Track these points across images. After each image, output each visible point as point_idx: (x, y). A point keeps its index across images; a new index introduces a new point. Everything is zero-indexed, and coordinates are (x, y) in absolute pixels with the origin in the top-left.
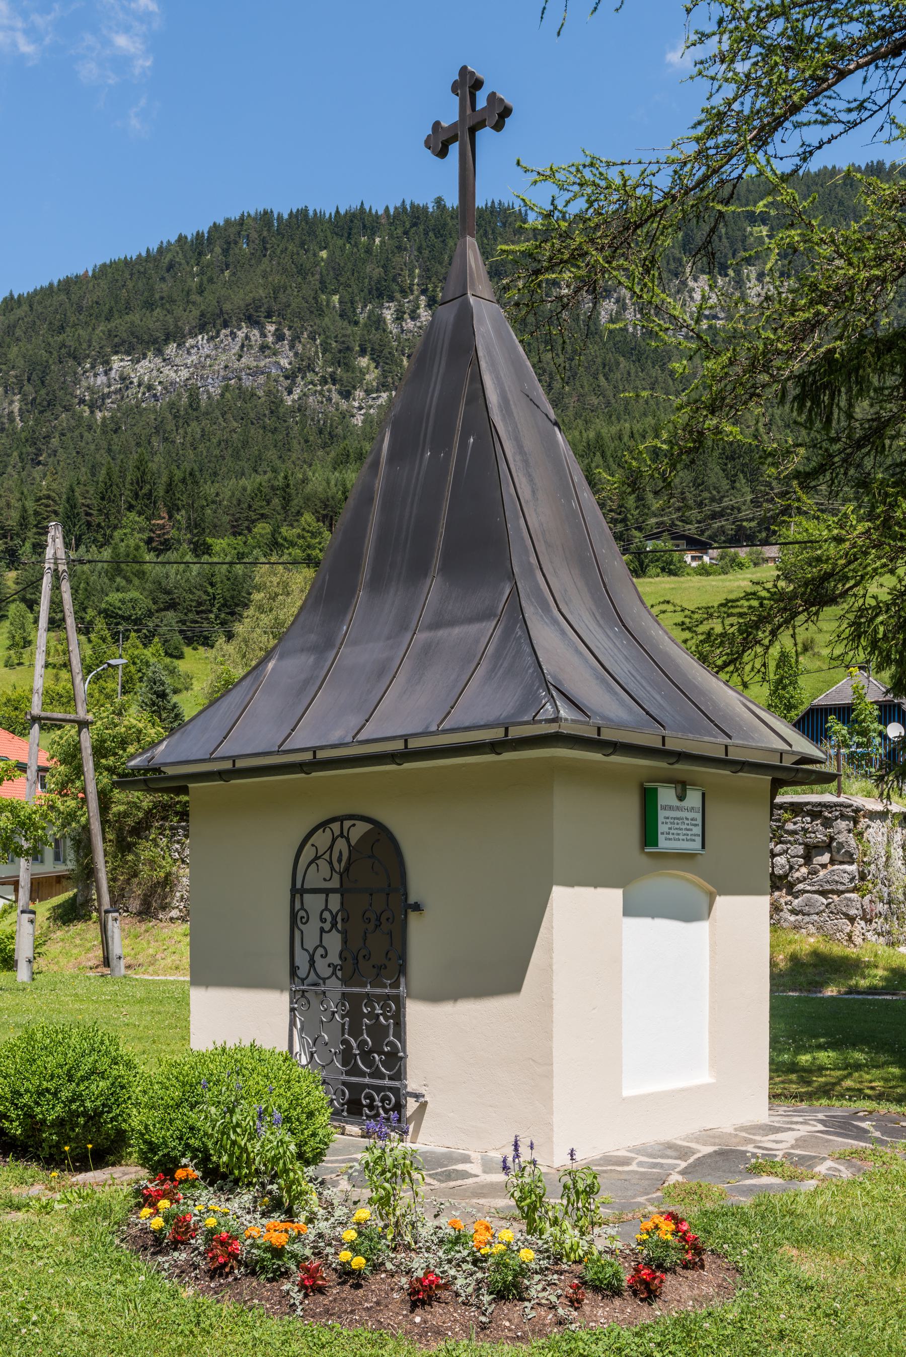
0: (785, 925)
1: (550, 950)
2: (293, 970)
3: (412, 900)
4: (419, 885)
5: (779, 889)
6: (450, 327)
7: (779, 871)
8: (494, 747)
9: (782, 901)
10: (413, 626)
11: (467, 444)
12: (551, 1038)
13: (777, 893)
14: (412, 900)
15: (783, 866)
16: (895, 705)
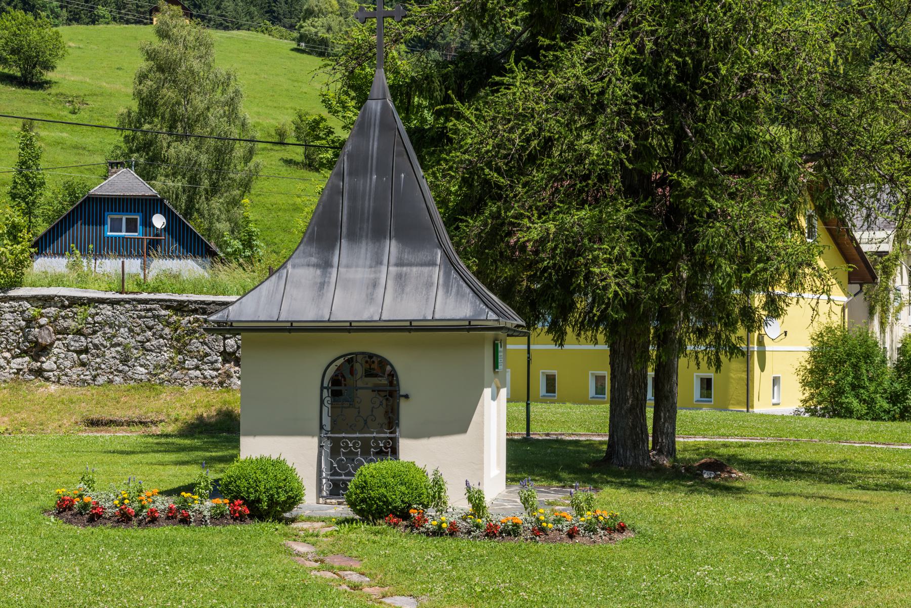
0: (235, 387)
1: (483, 415)
2: (321, 427)
3: (402, 393)
4: (405, 385)
5: (229, 362)
6: (378, 114)
7: (229, 350)
8: (469, 330)
9: (232, 370)
10: (385, 261)
11: (400, 177)
12: (482, 452)
13: (227, 365)
14: (402, 393)
15: (233, 346)
16: (158, 200)
